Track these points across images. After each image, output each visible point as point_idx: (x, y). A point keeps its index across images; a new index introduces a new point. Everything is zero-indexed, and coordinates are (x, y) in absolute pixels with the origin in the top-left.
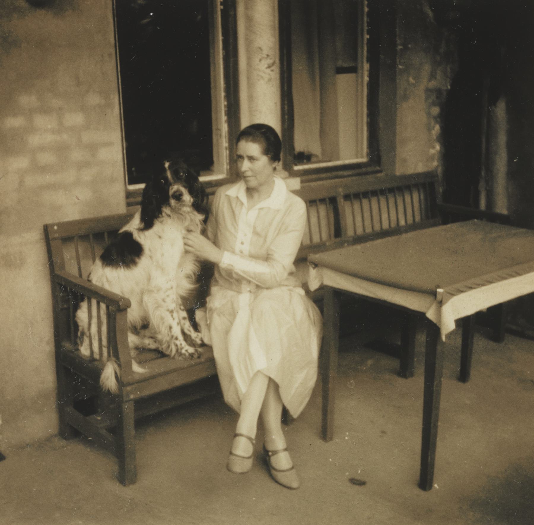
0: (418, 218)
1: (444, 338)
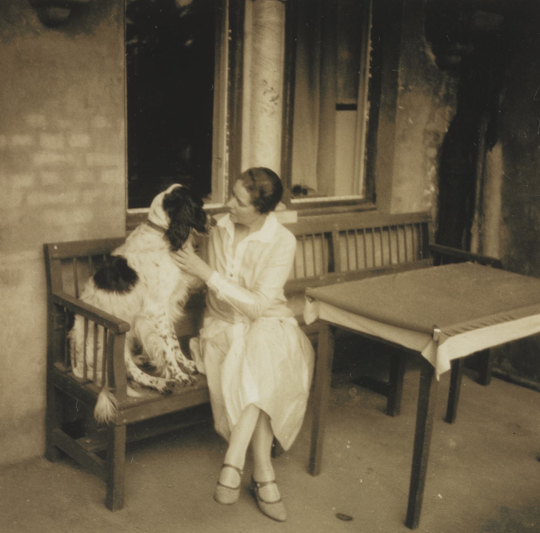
0: (410, 257)
1: (438, 378)
